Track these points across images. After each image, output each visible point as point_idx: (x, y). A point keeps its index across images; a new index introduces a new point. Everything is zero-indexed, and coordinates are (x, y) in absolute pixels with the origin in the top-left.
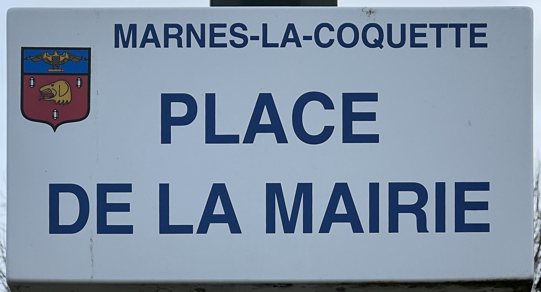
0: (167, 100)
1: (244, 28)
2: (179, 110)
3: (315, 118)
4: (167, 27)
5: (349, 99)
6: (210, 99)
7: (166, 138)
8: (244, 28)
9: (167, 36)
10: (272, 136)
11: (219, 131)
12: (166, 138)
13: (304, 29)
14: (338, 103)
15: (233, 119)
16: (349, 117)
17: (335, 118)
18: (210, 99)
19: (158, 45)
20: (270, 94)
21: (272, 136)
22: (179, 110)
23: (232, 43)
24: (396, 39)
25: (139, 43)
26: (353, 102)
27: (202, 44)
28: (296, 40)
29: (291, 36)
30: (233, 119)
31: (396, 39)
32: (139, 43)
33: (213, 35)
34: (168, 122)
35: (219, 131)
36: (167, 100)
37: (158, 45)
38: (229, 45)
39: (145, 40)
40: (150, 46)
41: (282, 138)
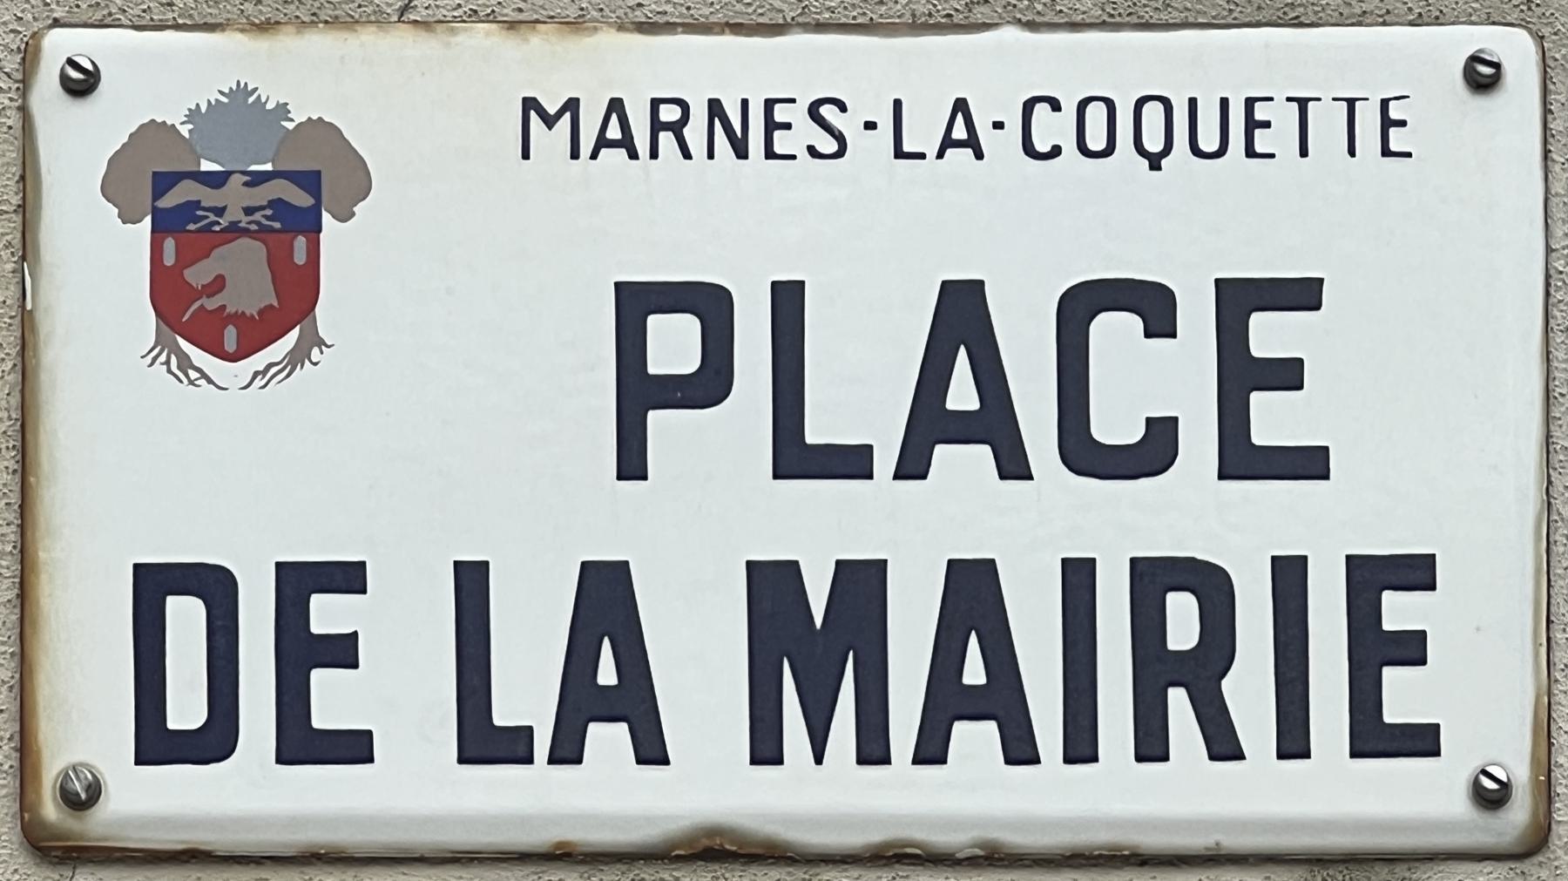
0: (636, 303)
1: (843, 107)
2: (674, 344)
4: (656, 103)
5: (1239, 300)
6: (788, 301)
8: (843, 107)
9: (657, 126)
10: (982, 454)
11: (907, 148)
13: (995, 104)
14: (1197, 316)
16: (1243, 375)
18: (788, 301)
19: (633, 155)
20: (945, 285)
21: (982, 454)
23: (813, 152)
25: (586, 146)
26: (170, 600)
28: (972, 143)
29: (962, 134)
30: (862, 384)
34: (639, 393)
35: (907, 148)
36: (636, 303)
37: (633, 155)
38: (803, 154)
39: (602, 142)
40: (614, 157)
41: (1013, 466)
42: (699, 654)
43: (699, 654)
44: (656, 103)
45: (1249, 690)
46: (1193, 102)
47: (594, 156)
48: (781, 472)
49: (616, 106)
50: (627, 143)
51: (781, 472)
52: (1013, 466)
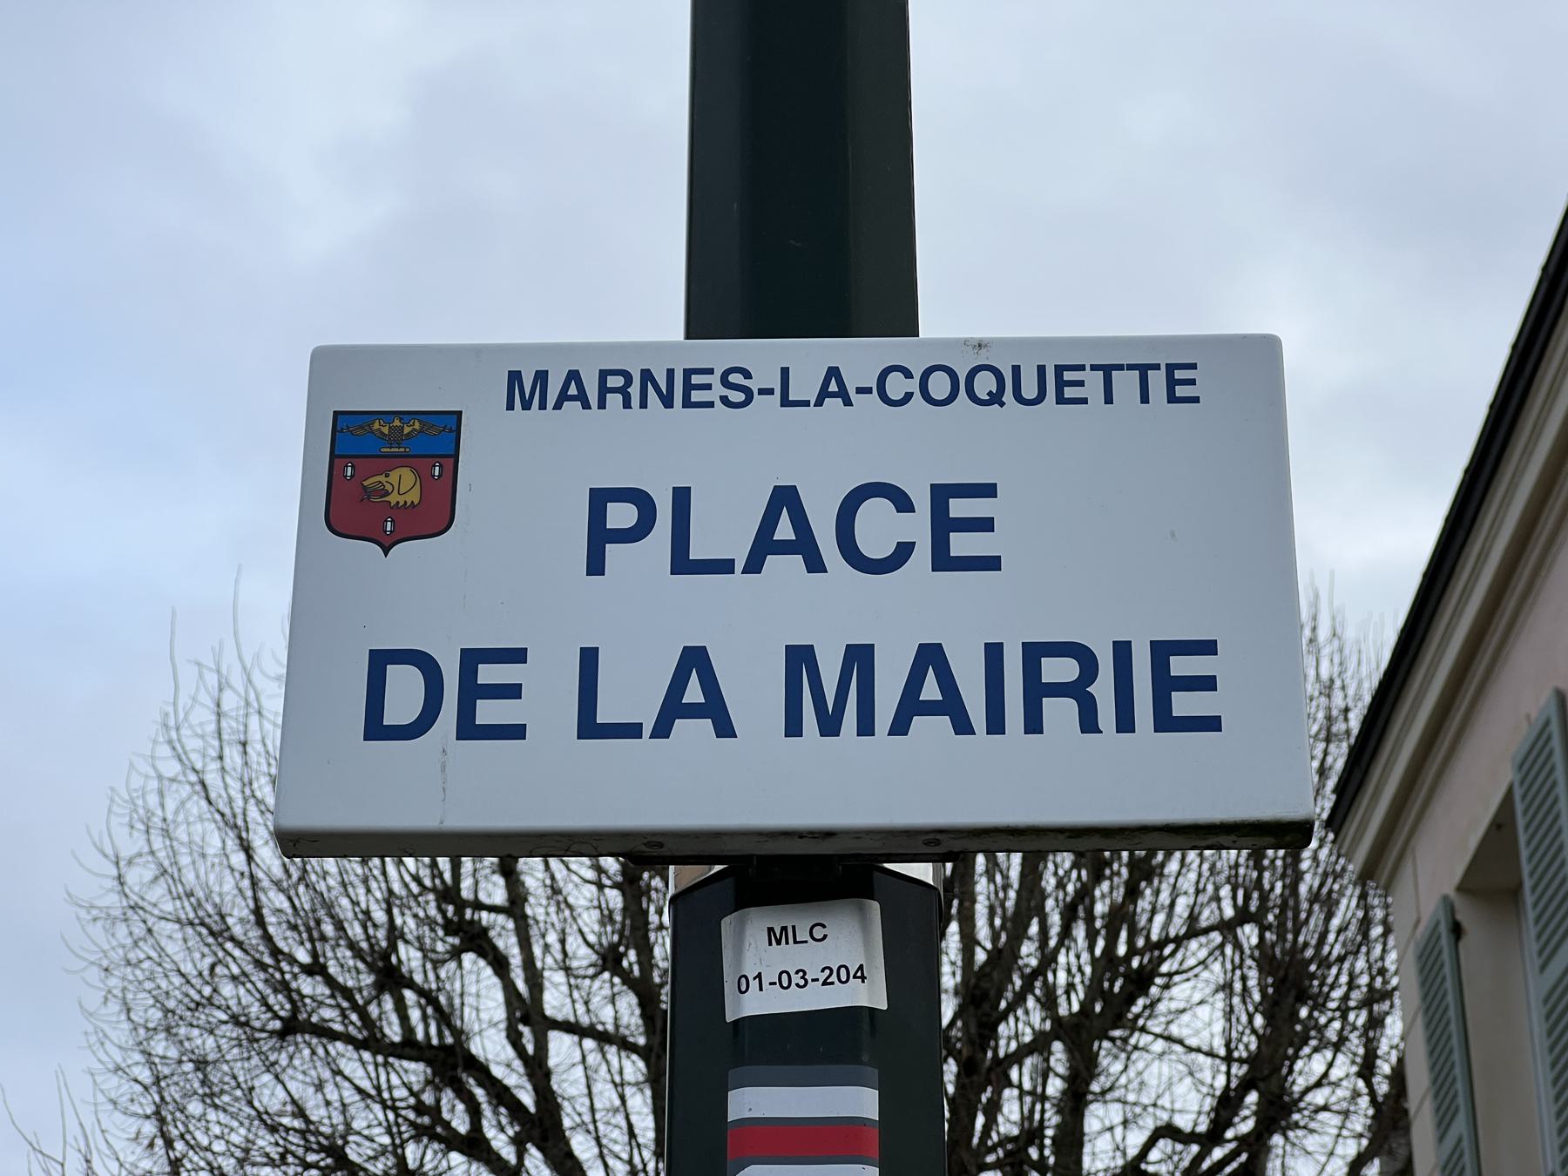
0: (600, 499)
2: (621, 516)
3: (878, 528)
4: (604, 374)
6: (682, 497)
7: (596, 565)
9: (604, 390)
12: (596, 565)
15: (723, 529)
17: (918, 527)
18: (682, 497)
19: (586, 406)
22: (621, 516)
24: (1030, 391)
25: (552, 399)
27: (668, 402)
30: (723, 529)
31: (1030, 391)
32: (552, 399)
33: (688, 387)
34: (600, 537)
36: (600, 499)
38: (718, 403)
41: (815, 564)
42: (754, 689)
43: (754, 689)
44: (604, 374)
45: (1103, 689)
46: (1145, 399)
47: (558, 406)
48: (374, 654)
49: (574, 376)
50: (582, 398)
51: (374, 654)
52: (815, 564)
